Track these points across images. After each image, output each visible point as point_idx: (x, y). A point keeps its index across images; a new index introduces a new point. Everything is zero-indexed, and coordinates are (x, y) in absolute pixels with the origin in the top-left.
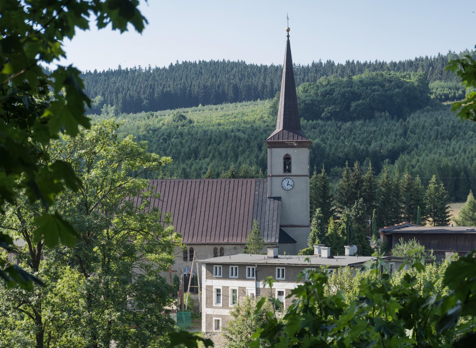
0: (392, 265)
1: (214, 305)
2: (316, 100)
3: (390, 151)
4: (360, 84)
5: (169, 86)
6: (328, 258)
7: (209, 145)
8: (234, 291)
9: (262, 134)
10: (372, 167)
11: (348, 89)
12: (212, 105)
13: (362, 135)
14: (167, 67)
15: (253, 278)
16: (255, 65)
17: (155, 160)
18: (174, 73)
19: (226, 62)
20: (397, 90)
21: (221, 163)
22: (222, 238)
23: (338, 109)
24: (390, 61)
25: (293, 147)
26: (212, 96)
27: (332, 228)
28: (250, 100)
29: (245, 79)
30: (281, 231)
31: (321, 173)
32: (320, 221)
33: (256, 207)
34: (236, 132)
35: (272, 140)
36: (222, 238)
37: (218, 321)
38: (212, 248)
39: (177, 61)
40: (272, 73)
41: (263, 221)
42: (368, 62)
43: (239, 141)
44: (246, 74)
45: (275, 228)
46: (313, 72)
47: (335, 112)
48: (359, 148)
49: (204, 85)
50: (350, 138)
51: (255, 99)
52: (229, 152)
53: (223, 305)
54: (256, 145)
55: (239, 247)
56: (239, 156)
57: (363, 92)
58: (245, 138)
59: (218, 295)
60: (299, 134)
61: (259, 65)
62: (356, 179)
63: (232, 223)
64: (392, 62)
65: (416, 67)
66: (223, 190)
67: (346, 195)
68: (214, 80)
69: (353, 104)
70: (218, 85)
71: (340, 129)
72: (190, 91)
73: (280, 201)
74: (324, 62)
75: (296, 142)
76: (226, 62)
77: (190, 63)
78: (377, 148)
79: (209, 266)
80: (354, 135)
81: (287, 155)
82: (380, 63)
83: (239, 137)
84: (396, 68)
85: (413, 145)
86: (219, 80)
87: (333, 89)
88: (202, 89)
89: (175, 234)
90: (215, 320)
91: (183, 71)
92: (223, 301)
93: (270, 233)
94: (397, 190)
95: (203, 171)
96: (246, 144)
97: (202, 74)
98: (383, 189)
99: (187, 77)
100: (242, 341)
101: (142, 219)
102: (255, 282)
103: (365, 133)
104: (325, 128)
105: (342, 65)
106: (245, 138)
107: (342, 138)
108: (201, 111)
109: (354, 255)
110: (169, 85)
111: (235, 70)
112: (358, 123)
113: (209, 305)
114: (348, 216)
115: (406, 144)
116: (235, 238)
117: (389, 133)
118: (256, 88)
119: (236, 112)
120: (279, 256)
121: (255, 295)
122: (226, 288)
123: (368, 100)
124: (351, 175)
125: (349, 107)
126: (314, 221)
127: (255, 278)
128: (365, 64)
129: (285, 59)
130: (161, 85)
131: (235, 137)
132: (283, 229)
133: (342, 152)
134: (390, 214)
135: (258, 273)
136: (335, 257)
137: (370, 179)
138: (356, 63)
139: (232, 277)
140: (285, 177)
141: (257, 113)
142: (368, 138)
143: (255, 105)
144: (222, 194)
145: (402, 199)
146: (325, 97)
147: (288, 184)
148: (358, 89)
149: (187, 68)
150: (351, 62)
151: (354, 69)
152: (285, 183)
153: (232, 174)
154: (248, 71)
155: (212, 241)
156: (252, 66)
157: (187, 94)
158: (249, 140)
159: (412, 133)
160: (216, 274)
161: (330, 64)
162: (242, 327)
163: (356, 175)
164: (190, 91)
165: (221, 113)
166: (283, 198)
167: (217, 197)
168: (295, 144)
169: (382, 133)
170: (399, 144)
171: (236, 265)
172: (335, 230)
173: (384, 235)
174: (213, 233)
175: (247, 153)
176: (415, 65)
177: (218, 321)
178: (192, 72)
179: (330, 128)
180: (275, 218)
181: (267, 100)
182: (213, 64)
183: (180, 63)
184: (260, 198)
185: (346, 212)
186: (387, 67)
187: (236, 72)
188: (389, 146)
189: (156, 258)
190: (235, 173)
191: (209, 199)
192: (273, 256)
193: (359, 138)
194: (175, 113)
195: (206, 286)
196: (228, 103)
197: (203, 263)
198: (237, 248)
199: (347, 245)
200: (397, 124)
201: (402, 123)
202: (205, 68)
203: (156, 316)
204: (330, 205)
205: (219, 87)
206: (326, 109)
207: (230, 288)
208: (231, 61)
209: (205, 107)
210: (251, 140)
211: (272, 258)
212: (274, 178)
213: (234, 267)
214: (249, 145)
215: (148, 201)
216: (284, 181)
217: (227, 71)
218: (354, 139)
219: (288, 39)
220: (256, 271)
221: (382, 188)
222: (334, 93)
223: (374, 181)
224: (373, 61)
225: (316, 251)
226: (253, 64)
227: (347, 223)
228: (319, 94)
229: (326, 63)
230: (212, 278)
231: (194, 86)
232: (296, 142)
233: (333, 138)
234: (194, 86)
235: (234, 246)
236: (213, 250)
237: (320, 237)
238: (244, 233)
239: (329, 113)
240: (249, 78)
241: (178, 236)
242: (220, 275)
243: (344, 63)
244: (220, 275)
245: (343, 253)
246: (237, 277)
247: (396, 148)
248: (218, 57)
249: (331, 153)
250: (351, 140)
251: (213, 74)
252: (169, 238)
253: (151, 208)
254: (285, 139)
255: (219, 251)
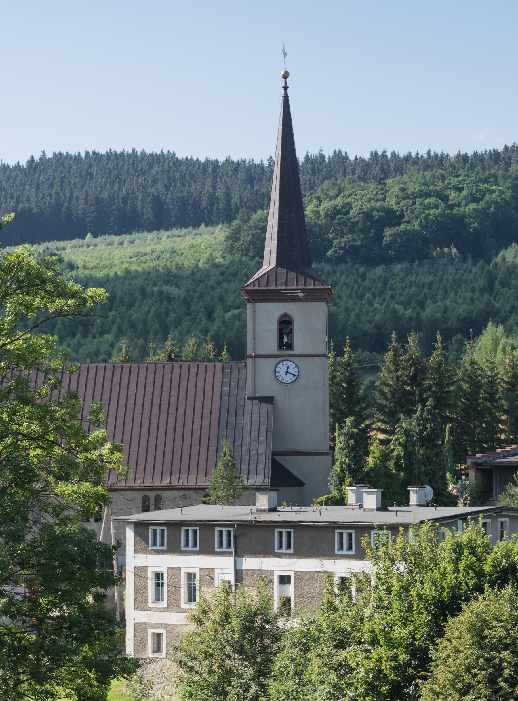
0: (502, 523)
1: (150, 604)
2: (316, 225)
3: (464, 320)
4: (400, 194)
5: (28, 200)
6: (378, 509)
7: (110, 310)
8: (191, 577)
9: (213, 288)
10: (442, 342)
11: (378, 204)
12: (112, 236)
13: (406, 291)
14: (24, 163)
15: (229, 550)
16: (195, 159)
17: (74, 295)
18: (37, 174)
19: (139, 154)
20: (472, 206)
21: (136, 343)
22: (158, 476)
23: (359, 242)
24: (456, 153)
25: (295, 299)
26: (112, 219)
27: (377, 455)
28: (186, 226)
29: (175, 186)
30: (274, 462)
31: (343, 356)
32: (353, 442)
33: (224, 416)
34: (162, 286)
35: (256, 287)
36: (158, 476)
37: (159, 635)
38: (138, 496)
39: (44, 152)
40: (227, 174)
41: (238, 443)
42: (414, 155)
43: (169, 302)
44: (178, 177)
45: (262, 458)
46: (308, 172)
47: (353, 247)
48: (404, 314)
49: (97, 198)
50: (383, 296)
51: (196, 225)
52: (150, 323)
53: (168, 605)
54: (203, 309)
55: (192, 493)
56: (171, 329)
57: (407, 208)
58: (179, 296)
59: (159, 585)
60: (307, 276)
61: (203, 160)
62: (411, 366)
63: (178, 448)
64: (459, 155)
65: (506, 164)
66: (158, 385)
67: (393, 397)
68: (116, 188)
69: (388, 233)
70: (124, 197)
71: (364, 280)
72: (69, 208)
73: (272, 404)
74: (328, 153)
75: (303, 291)
76: (139, 154)
77: (68, 157)
78: (439, 315)
79: (141, 528)
80: (392, 289)
81: (285, 315)
82: (436, 155)
83: (167, 294)
84: (468, 165)
85: (507, 308)
86: (125, 187)
87: (349, 203)
88: (92, 205)
89: (108, 445)
90: (153, 634)
91: (55, 171)
92: (168, 597)
93: (253, 466)
94: (492, 388)
95: (101, 357)
96: (183, 307)
97: (92, 176)
98: (465, 386)
99: (62, 182)
100: (211, 672)
101: (44, 414)
102: (232, 559)
103: (412, 286)
104: (335, 278)
105: (363, 160)
106: (179, 296)
107: (368, 295)
108: (91, 248)
109: (427, 505)
110: (29, 197)
111: (155, 169)
112: (398, 268)
113: (141, 603)
114: (407, 432)
115: (493, 306)
116: (184, 476)
117: (459, 286)
118: (197, 204)
119: (160, 247)
120: (279, 508)
121: (233, 582)
122: (174, 571)
123: (417, 224)
124: (401, 358)
125: (379, 237)
126: (340, 443)
127: (232, 549)
128: (408, 158)
129: (281, 131)
130: (12, 198)
131: (161, 293)
132: (278, 458)
133: (370, 322)
134: (479, 433)
135: (239, 540)
136: (390, 508)
137: (440, 366)
138: (389, 156)
139: (186, 549)
140: (281, 359)
141: (200, 250)
142: (418, 295)
143: (196, 234)
144: (157, 392)
145: (502, 405)
146: (333, 218)
147: (287, 372)
148: (398, 203)
149: (62, 165)
150: (380, 153)
151: (386, 167)
152: (282, 369)
153: (170, 356)
154: (182, 171)
155: (138, 483)
156: (189, 163)
157: (63, 214)
158: (189, 299)
159: (503, 287)
160: (155, 544)
161: (340, 158)
162: (213, 645)
163: (411, 358)
164: (69, 208)
165: (131, 250)
166: (279, 399)
167: (148, 397)
168: (301, 295)
169: (445, 288)
170: (480, 306)
171: (196, 525)
172: (385, 457)
173: (477, 470)
174: (141, 467)
175: (186, 324)
176: (504, 158)
177: (159, 635)
178: (72, 172)
179: (344, 277)
180: (262, 438)
181: (220, 226)
182: (113, 157)
183: (49, 155)
184: (233, 400)
185: (404, 425)
186: (451, 164)
187: (157, 173)
188: (461, 311)
189: (73, 491)
190: (175, 356)
191: (131, 401)
192: (267, 507)
193: (401, 295)
194: (41, 251)
195: (135, 567)
196: (143, 231)
197: (128, 522)
198: (188, 496)
199: (412, 484)
200: (474, 270)
201: (483, 268)
202: (98, 165)
203: (79, 604)
204: (361, 416)
205: (125, 201)
206: (335, 242)
207: (183, 571)
208: (148, 152)
209: (99, 239)
210: (192, 300)
211: (264, 511)
212: (259, 360)
213: (191, 529)
214: (188, 308)
215: (57, 379)
216: (280, 365)
217: (141, 170)
218: (392, 297)
219: (286, 93)
220: (235, 538)
221: (462, 383)
222: (351, 212)
223: (447, 371)
224: (423, 152)
225: (351, 497)
226: (191, 159)
227: (405, 446)
228: (322, 213)
229: (331, 155)
230: (146, 551)
231: (77, 198)
232: (303, 291)
233: (350, 296)
234: (77, 198)
235: (182, 493)
236: (140, 501)
237: (353, 473)
238: (202, 467)
239: (341, 248)
240: (184, 185)
241: (115, 449)
242: (162, 544)
243: (367, 157)
244: (162, 544)
245: (404, 501)
246: (197, 549)
247: (474, 315)
248: (122, 145)
249: (349, 323)
250: (388, 298)
251: (112, 176)
252: (95, 454)
253: (64, 391)
254: (282, 285)
255: (152, 502)
